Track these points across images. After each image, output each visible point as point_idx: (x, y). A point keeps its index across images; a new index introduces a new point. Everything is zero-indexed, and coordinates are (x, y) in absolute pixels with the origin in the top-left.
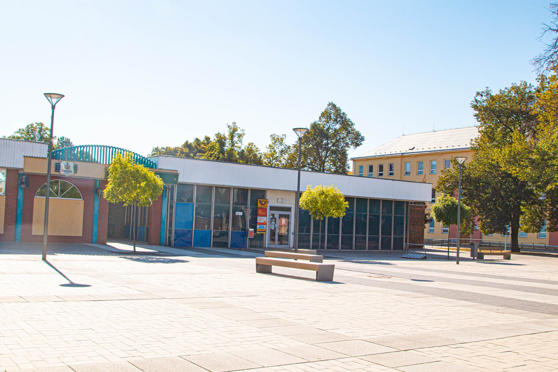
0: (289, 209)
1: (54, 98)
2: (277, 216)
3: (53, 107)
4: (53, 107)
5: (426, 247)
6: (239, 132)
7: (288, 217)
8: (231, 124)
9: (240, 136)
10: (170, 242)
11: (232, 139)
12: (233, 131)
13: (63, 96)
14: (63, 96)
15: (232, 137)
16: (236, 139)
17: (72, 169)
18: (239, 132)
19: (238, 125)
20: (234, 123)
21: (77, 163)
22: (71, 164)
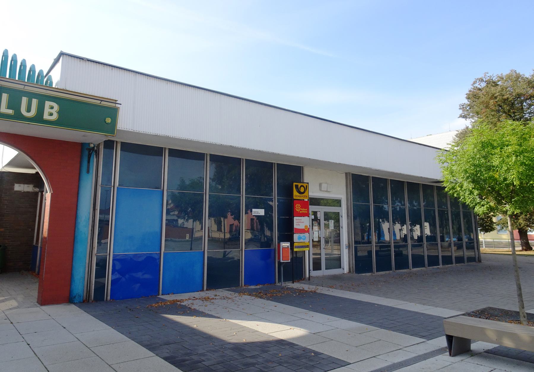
0: (338, 202)
2: (321, 216)
7: (337, 217)
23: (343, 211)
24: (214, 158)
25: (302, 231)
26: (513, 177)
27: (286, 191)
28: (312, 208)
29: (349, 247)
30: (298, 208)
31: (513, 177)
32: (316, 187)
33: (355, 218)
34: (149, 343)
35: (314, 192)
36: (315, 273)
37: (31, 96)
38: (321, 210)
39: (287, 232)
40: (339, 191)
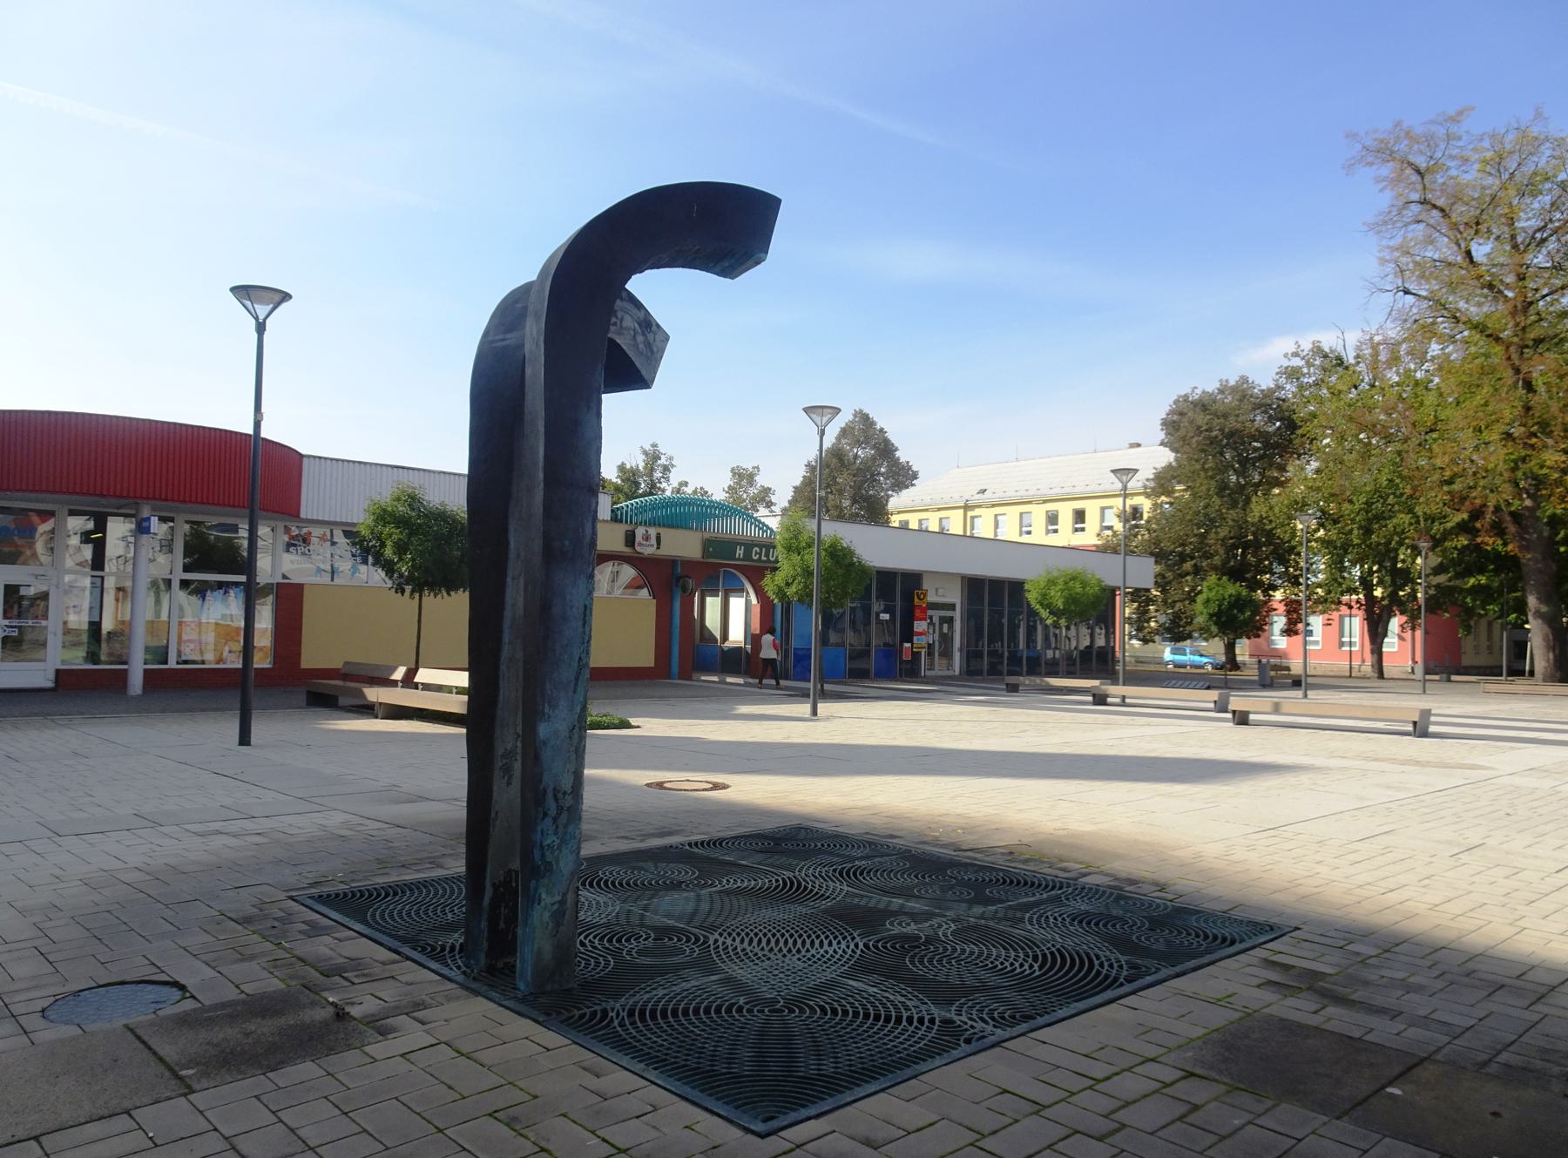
0: (952, 607)
1: (261, 302)
2: (936, 620)
3: (261, 328)
4: (261, 328)
5: (164, 617)
6: (663, 461)
7: (950, 620)
8: (648, 447)
9: (666, 469)
10: (787, 671)
11: (651, 475)
12: (653, 457)
13: (286, 297)
14: (286, 297)
15: (650, 470)
16: (658, 474)
17: (653, 541)
18: (663, 461)
19: (661, 449)
20: (654, 445)
21: (661, 530)
22: (653, 532)
23: (957, 615)
24: (1036, 666)
25: (920, 634)
26: (1060, 605)
27: (908, 597)
28: (930, 612)
29: (961, 650)
30: (918, 613)
31: (1060, 605)
32: (933, 593)
33: (1013, 689)
34: (275, 984)
35: (932, 598)
36: (929, 673)
37: (761, 546)
38: (936, 615)
39: (908, 635)
40: (954, 596)
